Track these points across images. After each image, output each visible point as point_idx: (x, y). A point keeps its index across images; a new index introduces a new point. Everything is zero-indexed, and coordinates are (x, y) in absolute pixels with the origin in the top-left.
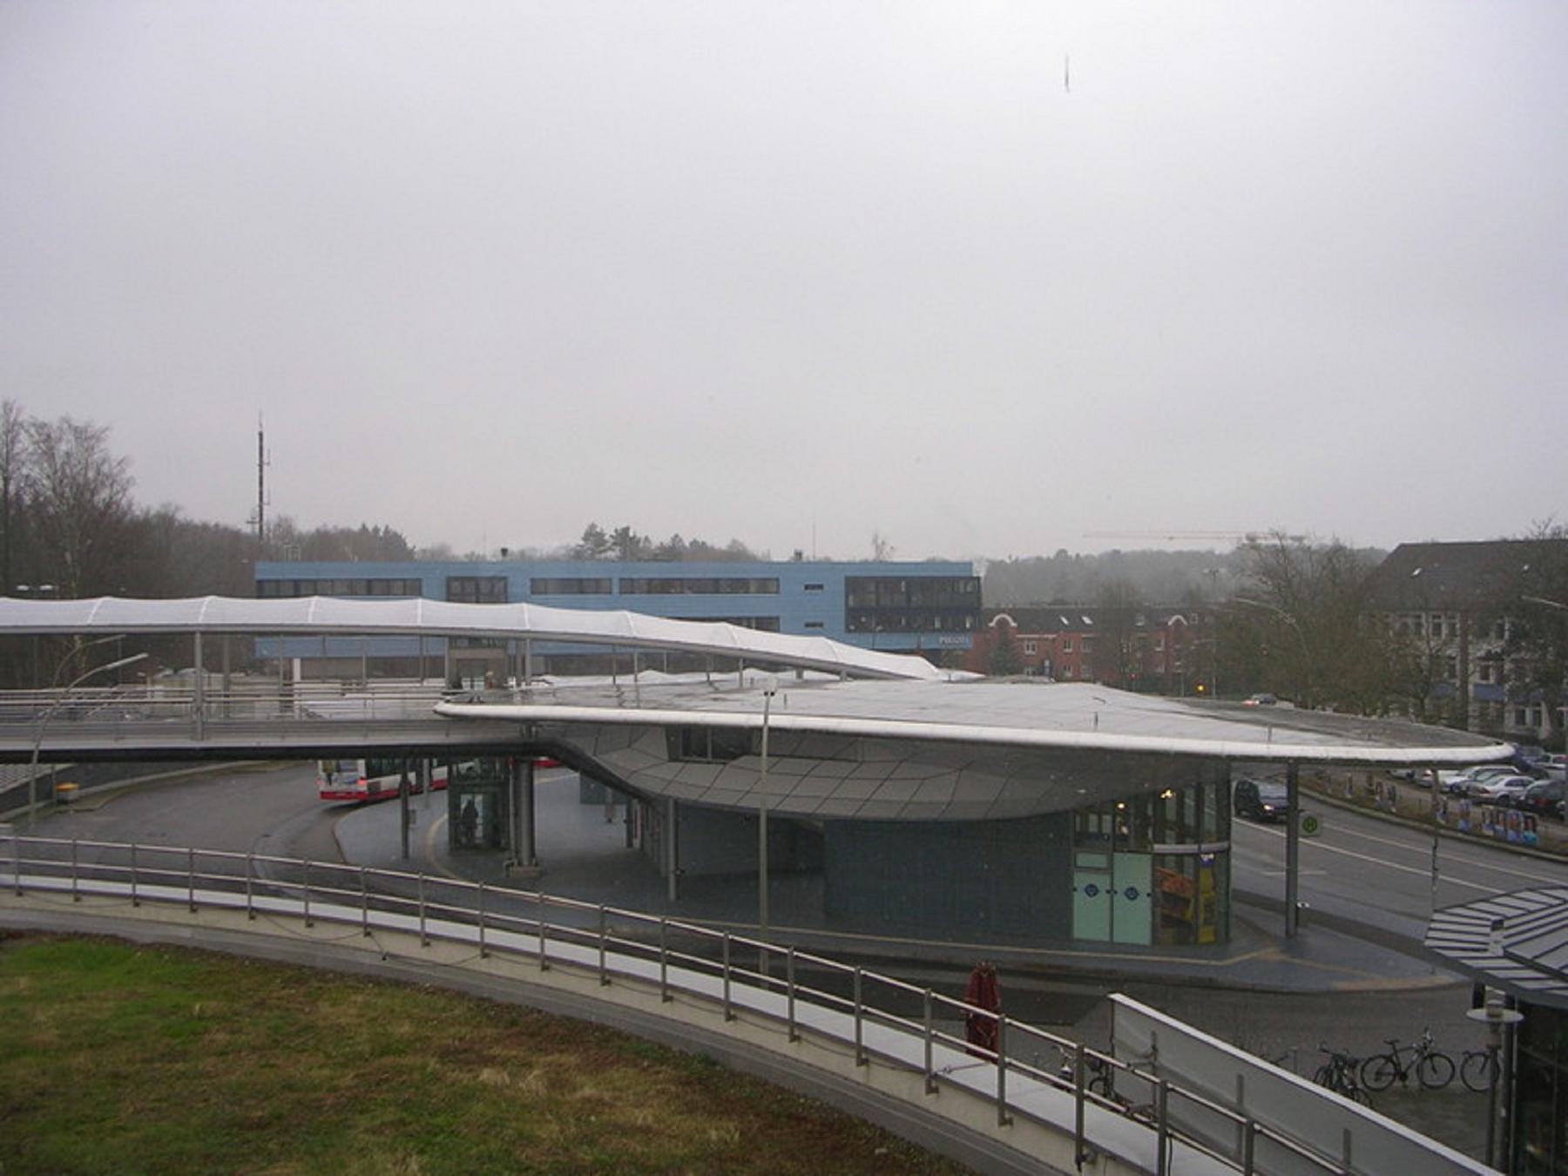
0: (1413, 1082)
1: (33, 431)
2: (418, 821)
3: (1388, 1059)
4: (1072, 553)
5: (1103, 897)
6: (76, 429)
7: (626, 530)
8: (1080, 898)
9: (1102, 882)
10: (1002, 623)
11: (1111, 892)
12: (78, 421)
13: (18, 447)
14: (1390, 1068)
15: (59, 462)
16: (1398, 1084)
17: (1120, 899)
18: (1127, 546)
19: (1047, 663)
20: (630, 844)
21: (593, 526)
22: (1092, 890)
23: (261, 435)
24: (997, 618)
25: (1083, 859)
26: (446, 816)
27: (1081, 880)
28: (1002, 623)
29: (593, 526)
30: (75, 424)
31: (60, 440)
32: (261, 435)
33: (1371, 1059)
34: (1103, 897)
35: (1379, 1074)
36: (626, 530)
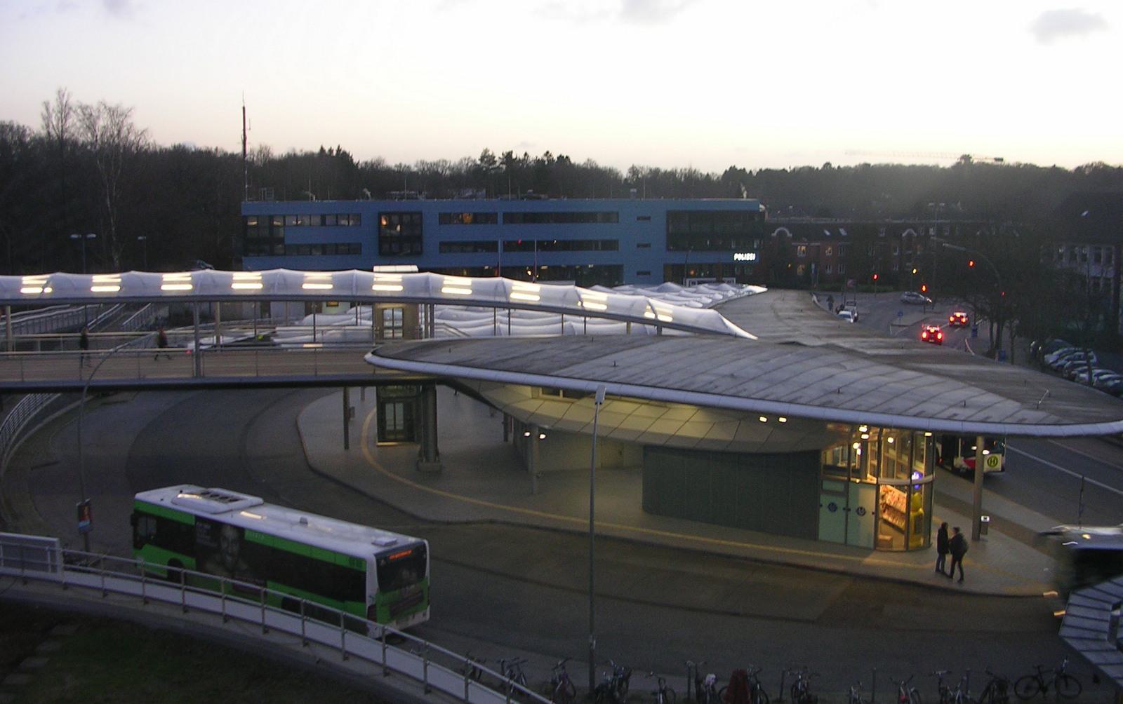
0: (1052, 693)
1: (79, 111)
2: (356, 415)
3: (1035, 678)
4: (835, 165)
5: (840, 514)
6: (110, 110)
7: (510, 154)
8: (824, 513)
9: (840, 502)
10: (781, 234)
11: (847, 510)
12: (112, 103)
13: (69, 122)
14: (1036, 684)
15: (99, 133)
16: (1040, 693)
17: (852, 514)
18: (873, 161)
19: (813, 266)
20: (506, 439)
21: (486, 151)
22: (833, 507)
23: (244, 108)
24: (778, 230)
25: (827, 485)
26: (375, 410)
27: (825, 500)
28: (781, 234)
29: (486, 151)
30: (109, 105)
31: (98, 117)
32: (244, 108)
33: (1021, 678)
34: (840, 514)
35: (1028, 688)
36: (510, 154)
